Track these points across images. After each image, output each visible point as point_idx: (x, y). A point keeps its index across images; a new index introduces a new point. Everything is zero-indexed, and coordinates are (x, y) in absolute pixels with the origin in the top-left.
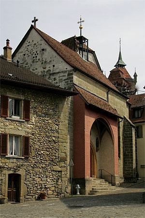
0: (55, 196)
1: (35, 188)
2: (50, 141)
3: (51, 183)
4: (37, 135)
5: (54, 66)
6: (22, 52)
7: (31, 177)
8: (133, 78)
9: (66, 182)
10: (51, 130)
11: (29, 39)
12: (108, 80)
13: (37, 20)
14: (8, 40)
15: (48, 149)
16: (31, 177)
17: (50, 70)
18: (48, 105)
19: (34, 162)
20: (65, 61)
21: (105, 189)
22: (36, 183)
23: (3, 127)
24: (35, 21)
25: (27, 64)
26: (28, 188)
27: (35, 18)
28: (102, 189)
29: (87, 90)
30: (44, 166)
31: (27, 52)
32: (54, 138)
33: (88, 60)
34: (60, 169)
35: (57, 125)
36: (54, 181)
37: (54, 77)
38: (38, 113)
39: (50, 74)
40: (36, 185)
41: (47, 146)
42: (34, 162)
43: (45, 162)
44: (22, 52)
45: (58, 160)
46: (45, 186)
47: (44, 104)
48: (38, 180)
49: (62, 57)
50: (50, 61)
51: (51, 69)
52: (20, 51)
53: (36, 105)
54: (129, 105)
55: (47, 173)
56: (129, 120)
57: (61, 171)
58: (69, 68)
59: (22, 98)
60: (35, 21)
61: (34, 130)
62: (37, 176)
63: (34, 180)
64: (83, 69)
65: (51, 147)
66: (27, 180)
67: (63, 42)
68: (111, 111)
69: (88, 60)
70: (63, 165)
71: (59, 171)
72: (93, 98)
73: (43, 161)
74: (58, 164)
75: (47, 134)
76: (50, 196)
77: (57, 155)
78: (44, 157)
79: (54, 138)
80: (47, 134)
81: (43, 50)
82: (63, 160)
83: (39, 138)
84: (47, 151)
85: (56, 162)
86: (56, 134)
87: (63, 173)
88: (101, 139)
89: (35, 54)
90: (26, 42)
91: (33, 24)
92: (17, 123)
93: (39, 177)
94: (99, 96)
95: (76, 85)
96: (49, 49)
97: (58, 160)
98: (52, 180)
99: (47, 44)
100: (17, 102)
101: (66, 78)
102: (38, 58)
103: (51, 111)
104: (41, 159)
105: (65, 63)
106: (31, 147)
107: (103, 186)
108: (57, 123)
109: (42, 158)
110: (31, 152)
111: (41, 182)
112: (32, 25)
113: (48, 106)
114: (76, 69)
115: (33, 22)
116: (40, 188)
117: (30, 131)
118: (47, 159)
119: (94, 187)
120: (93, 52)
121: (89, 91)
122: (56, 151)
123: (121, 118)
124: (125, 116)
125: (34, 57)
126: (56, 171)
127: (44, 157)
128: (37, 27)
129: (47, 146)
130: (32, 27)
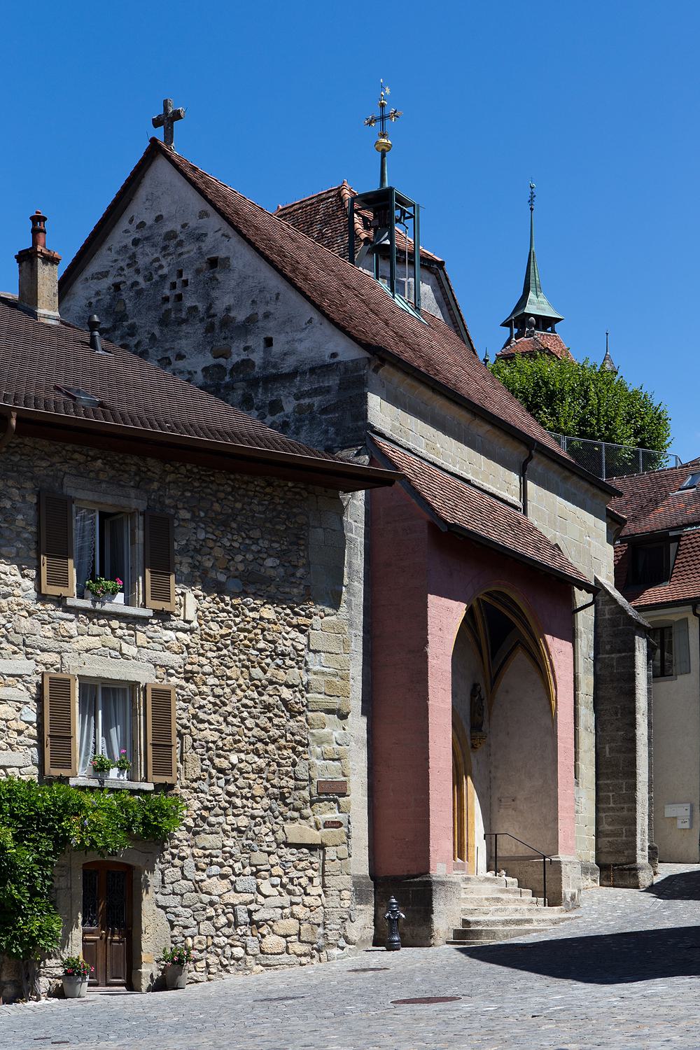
0: (294, 959)
1: (206, 927)
2: (268, 707)
3: (278, 901)
4: (212, 680)
5: (269, 342)
6: (105, 274)
7: (185, 878)
8: (530, 484)
9: (346, 894)
10: (275, 654)
11: (140, 210)
12: (74, 557)
13: (177, 115)
14: (37, 219)
15: (259, 745)
16: (185, 878)
17: (247, 363)
18: (256, 534)
19: (197, 805)
20: (327, 316)
21: (518, 922)
22: (212, 904)
23: (52, 644)
24: (167, 120)
25: (132, 335)
26: (172, 927)
27: (166, 104)
28: (506, 923)
29: (432, 457)
30: (243, 822)
31: (130, 276)
32: (286, 693)
33: (417, 309)
34: (314, 837)
35: (301, 629)
36: (290, 893)
37: (270, 398)
38: (212, 574)
39: (254, 383)
40: (210, 912)
41: (257, 731)
42: (197, 805)
43: (249, 803)
44: (105, 274)
45: (305, 794)
46: (250, 913)
47: (239, 529)
48: (219, 886)
49: (308, 298)
50: (251, 320)
51: (257, 358)
52: (95, 267)
53: (202, 536)
54: (615, 523)
55: (259, 857)
56: (616, 594)
57: (322, 847)
58: (348, 352)
59: (136, 502)
60: (167, 120)
61: (195, 658)
62: (215, 869)
63: (198, 887)
64: (407, 355)
65: (274, 732)
66: (169, 888)
67: (285, 214)
68: (545, 558)
69: (417, 309)
70: (333, 815)
71: (312, 847)
72: (461, 496)
73: (238, 802)
74: (307, 812)
75: (257, 672)
76: (273, 960)
77: (301, 769)
78: (241, 782)
79: (286, 693)
80: (257, 672)
81: (213, 263)
82: (334, 792)
83: (218, 691)
84: (256, 752)
85: (299, 804)
86: (294, 675)
87: (331, 853)
88: (495, 679)
89: (173, 286)
90: (124, 224)
91: (159, 134)
92: (115, 624)
93: (223, 877)
94: (487, 486)
95: (382, 435)
96: (241, 258)
97: (305, 794)
98: (283, 886)
99: (230, 232)
100: (110, 521)
101: (331, 398)
102: (189, 302)
103: (269, 562)
104: (229, 794)
105: (328, 329)
106: (180, 736)
107: (512, 907)
108: (302, 620)
109: (232, 788)
110: (182, 760)
111: (232, 898)
112: (153, 141)
113: (256, 542)
114: (380, 355)
115: (156, 123)
116: (228, 925)
117: (175, 660)
118: (258, 791)
119: (472, 912)
120: (433, 268)
121: (439, 461)
122: (298, 754)
123: (584, 586)
124: (601, 580)
125: (166, 299)
126: (298, 846)
127: (241, 782)
128: (176, 150)
129: (257, 731)
130: (155, 151)
